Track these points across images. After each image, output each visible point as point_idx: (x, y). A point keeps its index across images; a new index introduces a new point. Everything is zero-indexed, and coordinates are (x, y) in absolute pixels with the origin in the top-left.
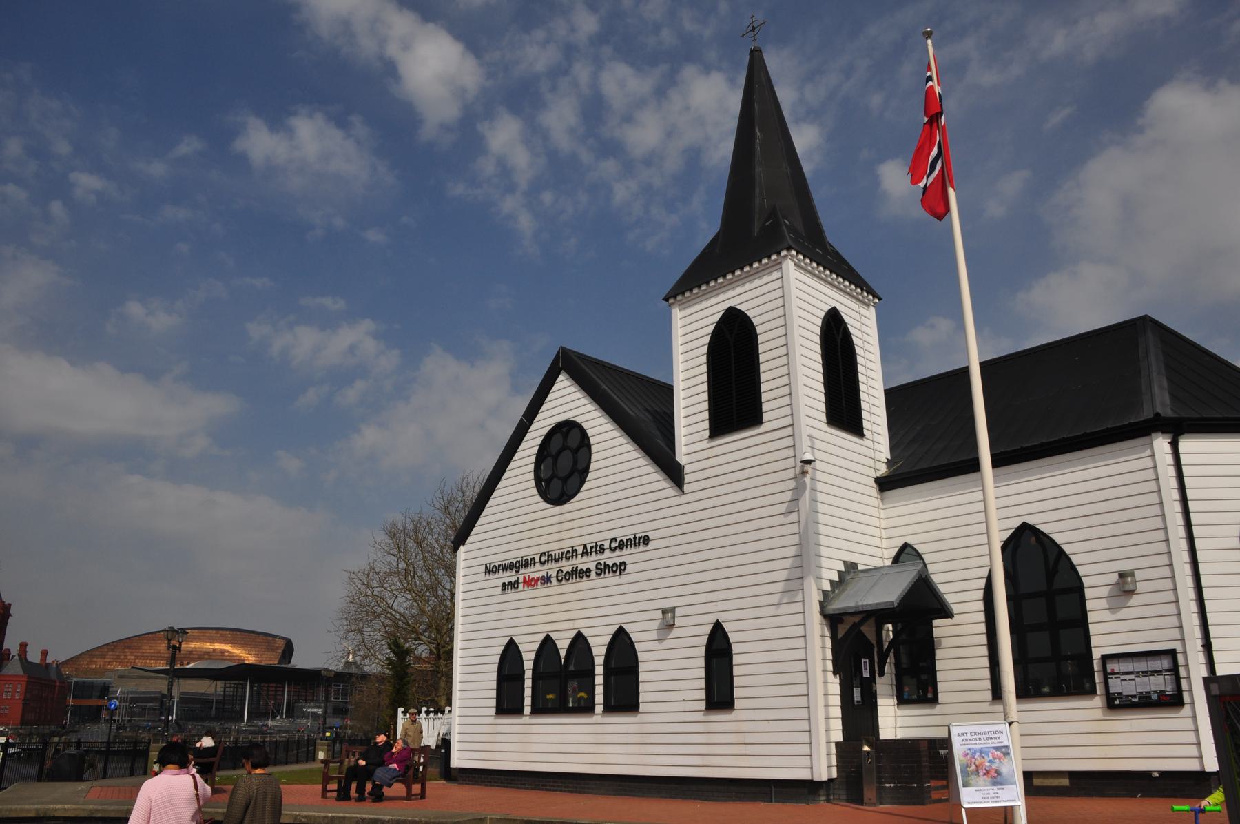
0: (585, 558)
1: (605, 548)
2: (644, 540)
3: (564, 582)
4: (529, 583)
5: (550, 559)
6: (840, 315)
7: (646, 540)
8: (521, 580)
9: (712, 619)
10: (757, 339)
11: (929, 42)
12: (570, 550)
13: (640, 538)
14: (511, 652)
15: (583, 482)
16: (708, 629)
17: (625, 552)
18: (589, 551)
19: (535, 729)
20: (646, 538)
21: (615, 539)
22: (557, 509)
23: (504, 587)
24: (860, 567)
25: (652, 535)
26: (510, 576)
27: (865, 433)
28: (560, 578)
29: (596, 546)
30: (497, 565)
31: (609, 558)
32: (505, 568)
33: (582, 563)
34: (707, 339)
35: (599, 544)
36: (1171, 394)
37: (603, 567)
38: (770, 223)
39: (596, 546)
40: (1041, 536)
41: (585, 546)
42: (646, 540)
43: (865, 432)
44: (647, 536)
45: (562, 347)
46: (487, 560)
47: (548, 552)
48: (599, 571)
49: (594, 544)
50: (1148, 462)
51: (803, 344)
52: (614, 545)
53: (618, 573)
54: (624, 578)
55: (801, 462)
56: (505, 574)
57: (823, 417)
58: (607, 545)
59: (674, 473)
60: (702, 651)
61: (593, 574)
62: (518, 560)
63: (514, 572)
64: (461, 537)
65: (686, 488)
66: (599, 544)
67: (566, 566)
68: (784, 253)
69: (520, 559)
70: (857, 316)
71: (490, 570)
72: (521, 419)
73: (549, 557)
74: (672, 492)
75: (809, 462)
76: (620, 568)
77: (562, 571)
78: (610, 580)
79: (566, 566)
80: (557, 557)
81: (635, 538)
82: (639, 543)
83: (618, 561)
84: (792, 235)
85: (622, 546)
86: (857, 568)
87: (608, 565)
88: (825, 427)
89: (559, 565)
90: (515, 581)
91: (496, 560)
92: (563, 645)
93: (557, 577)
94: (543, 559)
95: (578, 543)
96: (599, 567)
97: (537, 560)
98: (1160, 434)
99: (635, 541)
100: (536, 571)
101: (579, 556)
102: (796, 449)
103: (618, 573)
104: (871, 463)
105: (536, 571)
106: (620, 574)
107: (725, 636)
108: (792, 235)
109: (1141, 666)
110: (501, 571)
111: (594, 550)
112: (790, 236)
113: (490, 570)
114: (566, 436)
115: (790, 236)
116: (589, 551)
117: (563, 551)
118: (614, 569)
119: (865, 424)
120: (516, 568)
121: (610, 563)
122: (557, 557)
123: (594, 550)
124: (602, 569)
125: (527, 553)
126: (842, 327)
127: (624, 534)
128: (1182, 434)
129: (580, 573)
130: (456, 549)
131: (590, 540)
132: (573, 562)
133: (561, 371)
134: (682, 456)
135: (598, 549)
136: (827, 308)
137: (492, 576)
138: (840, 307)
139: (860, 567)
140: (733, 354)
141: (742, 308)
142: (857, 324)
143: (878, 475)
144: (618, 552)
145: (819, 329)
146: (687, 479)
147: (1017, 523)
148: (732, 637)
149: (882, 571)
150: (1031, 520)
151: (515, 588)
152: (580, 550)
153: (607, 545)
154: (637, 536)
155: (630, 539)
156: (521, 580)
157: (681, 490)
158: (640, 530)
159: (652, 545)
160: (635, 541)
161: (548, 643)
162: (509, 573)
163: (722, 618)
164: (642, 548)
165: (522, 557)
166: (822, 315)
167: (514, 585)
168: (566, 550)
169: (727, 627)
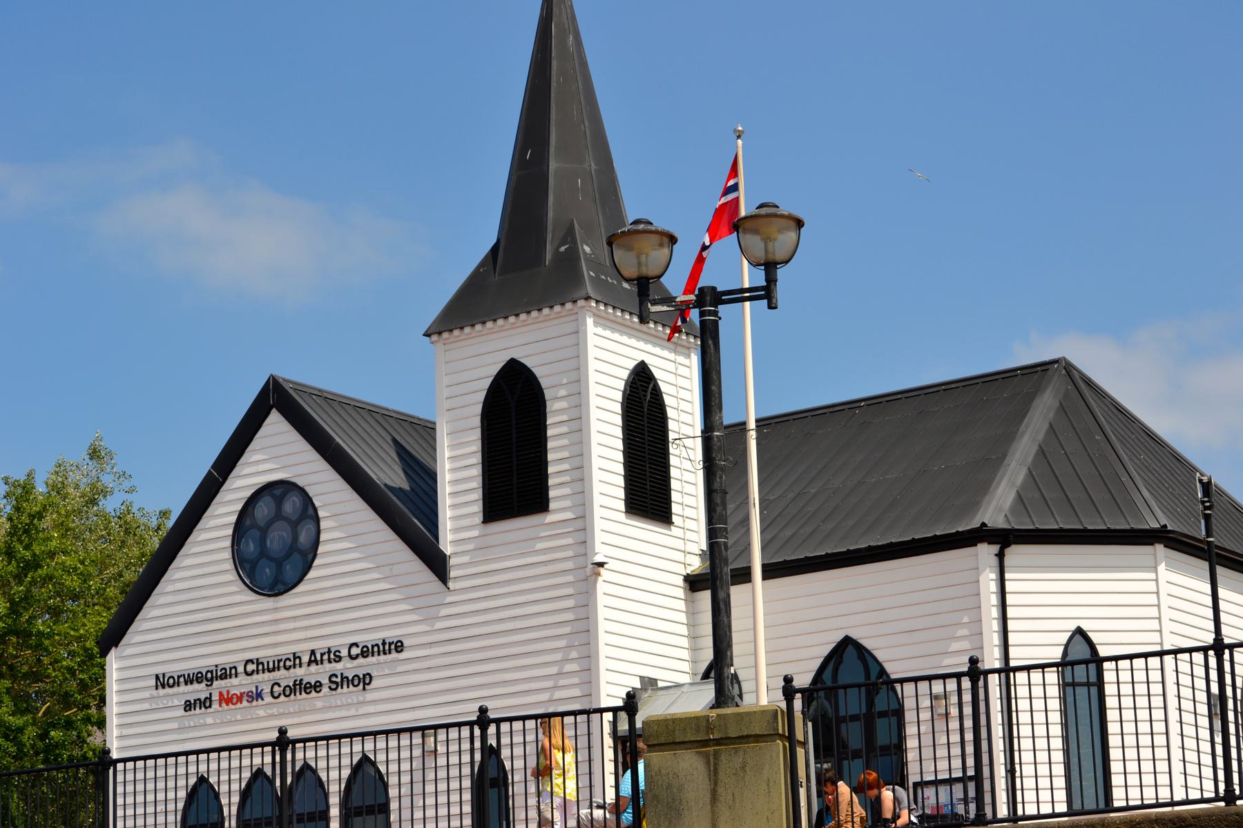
0: (313, 668)
1: (341, 655)
2: (396, 647)
3: (282, 698)
4: (227, 699)
5: (261, 667)
6: (648, 368)
8: (215, 697)
11: (740, 141)
12: (291, 657)
13: (390, 644)
15: (308, 567)
17: (370, 659)
18: (319, 658)
19: (544, 697)
20: (399, 644)
21: (356, 645)
22: (269, 603)
23: (188, 706)
24: (660, 684)
26: (198, 691)
27: (673, 521)
28: (276, 695)
29: (329, 652)
31: (347, 667)
32: (189, 681)
35: (333, 650)
36: (1019, 497)
37: (339, 680)
38: (566, 249)
39: (329, 652)
40: (864, 652)
41: (313, 652)
42: (399, 647)
43: (674, 518)
44: (400, 642)
45: (271, 375)
46: (160, 670)
47: (257, 659)
48: (334, 686)
49: (327, 650)
51: (608, 656)
52: (355, 651)
53: (361, 686)
55: (592, 564)
56: (190, 688)
57: (621, 506)
58: (344, 653)
59: (437, 564)
61: (325, 690)
62: (210, 669)
63: (203, 685)
64: (112, 637)
65: (451, 585)
66: (333, 650)
67: (285, 677)
68: (581, 303)
69: (214, 668)
70: (671, 367)
71: (162, 682)
72: (210, 471)
73: (260, 666)
74: (438, 584)
75: (601, 565)
76: (365, 680)
77: (279, 686)
79: (285, 677)
80: (271, 666)
81: (384, 643)
82: (390, 650)
84: (592, 273)
85: (365, 653)
86: (657, 685)
87: (347, 678)
88: (622, 517)
89: (276, 675)
90: (206, 698)
93: (272, 692)
94: (251, 667)
95: (303, 649)
96: (334, 679)
97: (241, 669)
98: (987, 544)
99: (384, 647)
100: (237, 684)
101: (304, 666)
102: (588, 546)
103: (361, 686)
104: (679, 556)
105: (237, 684)
106: (364, 689)
108: (592, 273)
110: (182, 684)
111: (326, 657)
112: (589, 274)
113: (162, 682)
114: (279, 501)
115: (589, 274)
116: (319, 658)
117: (280, 658)
118: (356, 683)
119: (675, 508)
120: (207, 680)
122: (271, 666)
123: (326, 657)
124: (338, 682)
126: (651, 386)
128: (1009, 545)
129: (306, 688)
130: (104, 653)
132: (299, 672)
133: (272, 409)
134: (448, 542)
135: (332, 656)
136: (631, 365)
137: (168, 690)
138: (650, 361)
139: (660, 684)
140: (514, 421)
142: (671, 378)
143: (689, 572)
144: (361, 660)
145: (619, 406)
146: (453, 573)
147: (838, 637)
149: (683, 689)
150: (854, 635)
151: (206, 708)
152: (305, 659)
153: (344, 653)
154: (387, 641)
155: (377, 645)
156: (215, 697)
157: (446, 586)
158: (391, 635)
160: (384, 647)
162: (196, 686)
164: (394, 655)
165: (216, 666)
166: (625, 374)
167: (206, 703)
168: (284, 657)
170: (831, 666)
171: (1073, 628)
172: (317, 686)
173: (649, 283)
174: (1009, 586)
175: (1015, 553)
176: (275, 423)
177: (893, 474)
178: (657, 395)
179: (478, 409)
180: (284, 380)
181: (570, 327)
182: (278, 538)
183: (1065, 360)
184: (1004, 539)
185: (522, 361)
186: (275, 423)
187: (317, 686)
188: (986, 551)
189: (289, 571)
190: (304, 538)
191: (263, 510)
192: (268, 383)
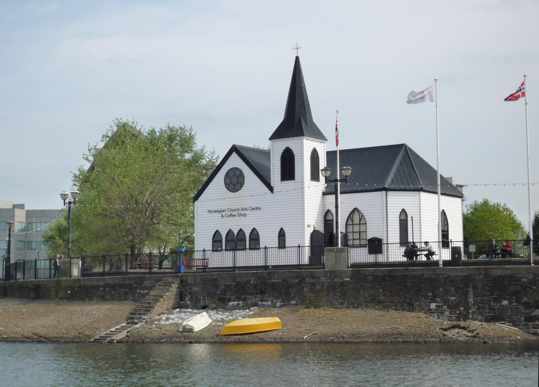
7: (467, 186)
9: (280, 227)
10: (294, 158)
14: (217, 233)
16: (279, 229)
25: (261, 207)
30: (212, 210)
31: (243, 212)
33: (234, 213)
34: (281, 154)
41: (242, 208)
42: (260, 208)
43: (320, 180)
46: (209, 209)
50: (418, 197)
54: (246, 218)
58: (248, 209)
59: (271, 189)
60: (277, 235)
61: (237, 216)
76: (245, 215)
78: (242, 218)
83: (244, 213)
91: (212, 209)
92: (236, 233)
107: (283, 231)
109: (298, 261)
121: (242, 213)
124: (240, 215)
125: (223, 208)
127: (254, 206)
131: (244, 207)
132: (239, 212)
136: (312, 148)
141: (291, 148)
146: (274, 191)
147: (354, 207)
148: (260, 236)
150: (357, 207)
152: (240, 209)
153: (248, 209)
159: (261, 210)
161: (230, 232)
163: (283, 227)
164: (259, 210)
166: (311, 151)
169: (284, 229)
170: (352, 213)
171: (402, 208)
172: (235, 216)
173: (378, 262)
174: (388, 200)
175: (389, 193)
176: (234, 155)
177: (245, 372)
178: (317, 154)
179: (280, 156)
180: (236, 145)
181: (300, 141)
182: (234, 180)
183: (406, 148)
184: (386, 190)
185: (290, 147)
186: (234, 155)
187: (235, 216)
188: (384, 192)
189: (237, 188)
190: (240, 181)
191: (231, 174)
192: (233, 146)
